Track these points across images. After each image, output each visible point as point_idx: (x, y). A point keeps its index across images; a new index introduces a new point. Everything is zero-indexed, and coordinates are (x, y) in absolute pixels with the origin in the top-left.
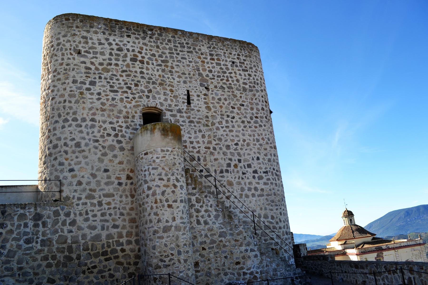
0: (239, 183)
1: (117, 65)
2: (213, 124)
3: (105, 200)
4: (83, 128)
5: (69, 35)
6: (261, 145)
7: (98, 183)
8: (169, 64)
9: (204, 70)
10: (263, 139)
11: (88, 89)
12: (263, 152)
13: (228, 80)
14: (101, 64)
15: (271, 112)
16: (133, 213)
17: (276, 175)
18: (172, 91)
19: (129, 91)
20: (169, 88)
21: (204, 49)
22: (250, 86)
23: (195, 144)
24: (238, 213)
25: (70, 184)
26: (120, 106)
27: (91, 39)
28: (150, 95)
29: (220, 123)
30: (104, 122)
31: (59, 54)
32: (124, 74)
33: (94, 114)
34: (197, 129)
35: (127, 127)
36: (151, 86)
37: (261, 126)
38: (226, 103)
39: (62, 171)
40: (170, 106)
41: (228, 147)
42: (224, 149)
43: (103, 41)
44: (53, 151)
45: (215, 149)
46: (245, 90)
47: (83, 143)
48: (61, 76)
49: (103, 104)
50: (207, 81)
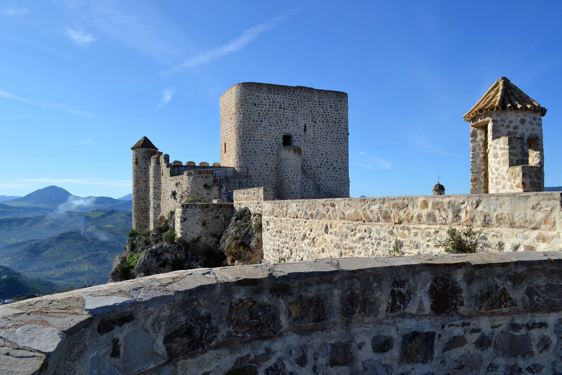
0: (325, 173)
1: (272, 111)
2: (316, 142)
3: (266, 177)
7: (263, 169)
8: (297, 109)
9: (315, 112)
11: (259, 125)
12: (340, 158)
14: (265, 111)
16: (277, 184)
18: (297, 124)
20: (296, 123)
21: (316, 99)
23: (306, 153)
25: (252, 170)
29: (320, 141)
30: (266, 141)
31: (246, 105)
33: (262, 137)
34: (308, 145)
36: (288, 122)
39: (248, 163)
40: (296, 132)
41: (322, 155)
42: (320, 156)
43: (266, 98)
44: (244, 154)
45: (315, 155)
46: (335, 122)
49: (266, 132)
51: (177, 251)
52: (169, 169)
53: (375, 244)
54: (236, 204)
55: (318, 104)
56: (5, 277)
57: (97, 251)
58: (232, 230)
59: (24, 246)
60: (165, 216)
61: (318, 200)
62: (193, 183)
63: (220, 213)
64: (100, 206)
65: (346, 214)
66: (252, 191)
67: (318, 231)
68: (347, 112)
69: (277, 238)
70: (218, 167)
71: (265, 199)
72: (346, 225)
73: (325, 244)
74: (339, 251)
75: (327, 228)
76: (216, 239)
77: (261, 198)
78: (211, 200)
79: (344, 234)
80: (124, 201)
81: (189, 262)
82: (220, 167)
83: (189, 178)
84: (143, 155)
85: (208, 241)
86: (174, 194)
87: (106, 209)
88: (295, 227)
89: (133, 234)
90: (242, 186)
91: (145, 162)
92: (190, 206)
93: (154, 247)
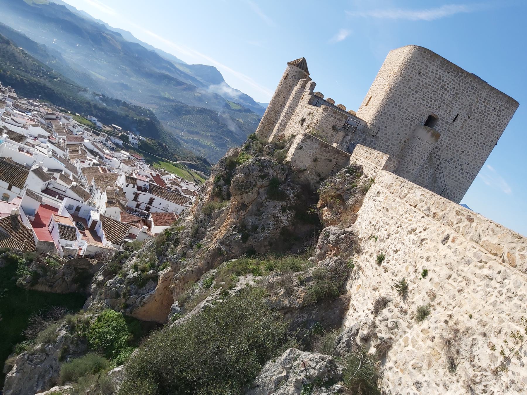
1: (433, 87)
3: (391, 146)
4: (400, 112)
5: (421, 61)
6: (475, 159)
8: (459, 96)
9: (475, 106)
10: (479, 156)
11: (413, 94)
12: (474, 162)
13: (484, 117)
15: (496, 144)
17: (472, 177)
18: (450, 111)
19: (430, 103)
20: (449, 109)
21: (484, 95)
22: (494, 126)
23: (443, 142)
24: (439, 182)
25: (382, 133)
26: (422, 108)
27: (430, 68)
28: (438, 109)
31: (411, 69)
32: (433, 93)
33: (408, 107)
35: (418, 120)
36: (442, 104)
37: (483, 149)
38: (474, 129)
42: (455, 151)
43: (434, 71)
44: (383, 115)
45: (450, 148)
46: (490, 126)
47: (397, 118)
48: (405, 82)
49: (415, 104)
50: (472, 113)
51: (280, 171)
52: (310, 97)
53: (504, 296)
54: (353, 157)
55: (483, 100)
56: (149, 119)
57: (222, 135)
58: (337, 179)
59: (172, 103)
60: (286, 136)
61: (452, 203)
62: (325, 119)
63: (334, 158)
64: (242, 101)
65: (483, 239)
66: (376, 154)
67: (433, 235)
68: (508, 122)
69: (380, 214)
70: (352, 115)
71: (385, 168)
72: (476, 250)
73: (434, 254)
74: (450, 272)
75: (447, 238)
76: (318, 179)
77: (381, 164)
78: (332, 142)
79: (467, 258)
80: (261, 107)
81: (285, 186)
82: (355, 116)
83: (323, 113)
84: (295, 74)
85: (310, 177)
86: (303, 120)
87: (246, 106)
88: (407, 215)
89: (253, 138)
90: (365, 143)
91: (293, 80)
92: (312, 138)
93: (263, 158)
